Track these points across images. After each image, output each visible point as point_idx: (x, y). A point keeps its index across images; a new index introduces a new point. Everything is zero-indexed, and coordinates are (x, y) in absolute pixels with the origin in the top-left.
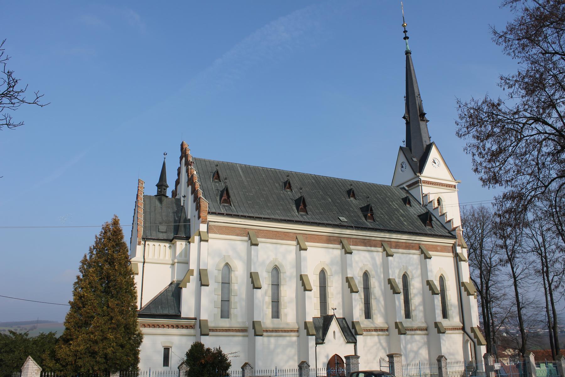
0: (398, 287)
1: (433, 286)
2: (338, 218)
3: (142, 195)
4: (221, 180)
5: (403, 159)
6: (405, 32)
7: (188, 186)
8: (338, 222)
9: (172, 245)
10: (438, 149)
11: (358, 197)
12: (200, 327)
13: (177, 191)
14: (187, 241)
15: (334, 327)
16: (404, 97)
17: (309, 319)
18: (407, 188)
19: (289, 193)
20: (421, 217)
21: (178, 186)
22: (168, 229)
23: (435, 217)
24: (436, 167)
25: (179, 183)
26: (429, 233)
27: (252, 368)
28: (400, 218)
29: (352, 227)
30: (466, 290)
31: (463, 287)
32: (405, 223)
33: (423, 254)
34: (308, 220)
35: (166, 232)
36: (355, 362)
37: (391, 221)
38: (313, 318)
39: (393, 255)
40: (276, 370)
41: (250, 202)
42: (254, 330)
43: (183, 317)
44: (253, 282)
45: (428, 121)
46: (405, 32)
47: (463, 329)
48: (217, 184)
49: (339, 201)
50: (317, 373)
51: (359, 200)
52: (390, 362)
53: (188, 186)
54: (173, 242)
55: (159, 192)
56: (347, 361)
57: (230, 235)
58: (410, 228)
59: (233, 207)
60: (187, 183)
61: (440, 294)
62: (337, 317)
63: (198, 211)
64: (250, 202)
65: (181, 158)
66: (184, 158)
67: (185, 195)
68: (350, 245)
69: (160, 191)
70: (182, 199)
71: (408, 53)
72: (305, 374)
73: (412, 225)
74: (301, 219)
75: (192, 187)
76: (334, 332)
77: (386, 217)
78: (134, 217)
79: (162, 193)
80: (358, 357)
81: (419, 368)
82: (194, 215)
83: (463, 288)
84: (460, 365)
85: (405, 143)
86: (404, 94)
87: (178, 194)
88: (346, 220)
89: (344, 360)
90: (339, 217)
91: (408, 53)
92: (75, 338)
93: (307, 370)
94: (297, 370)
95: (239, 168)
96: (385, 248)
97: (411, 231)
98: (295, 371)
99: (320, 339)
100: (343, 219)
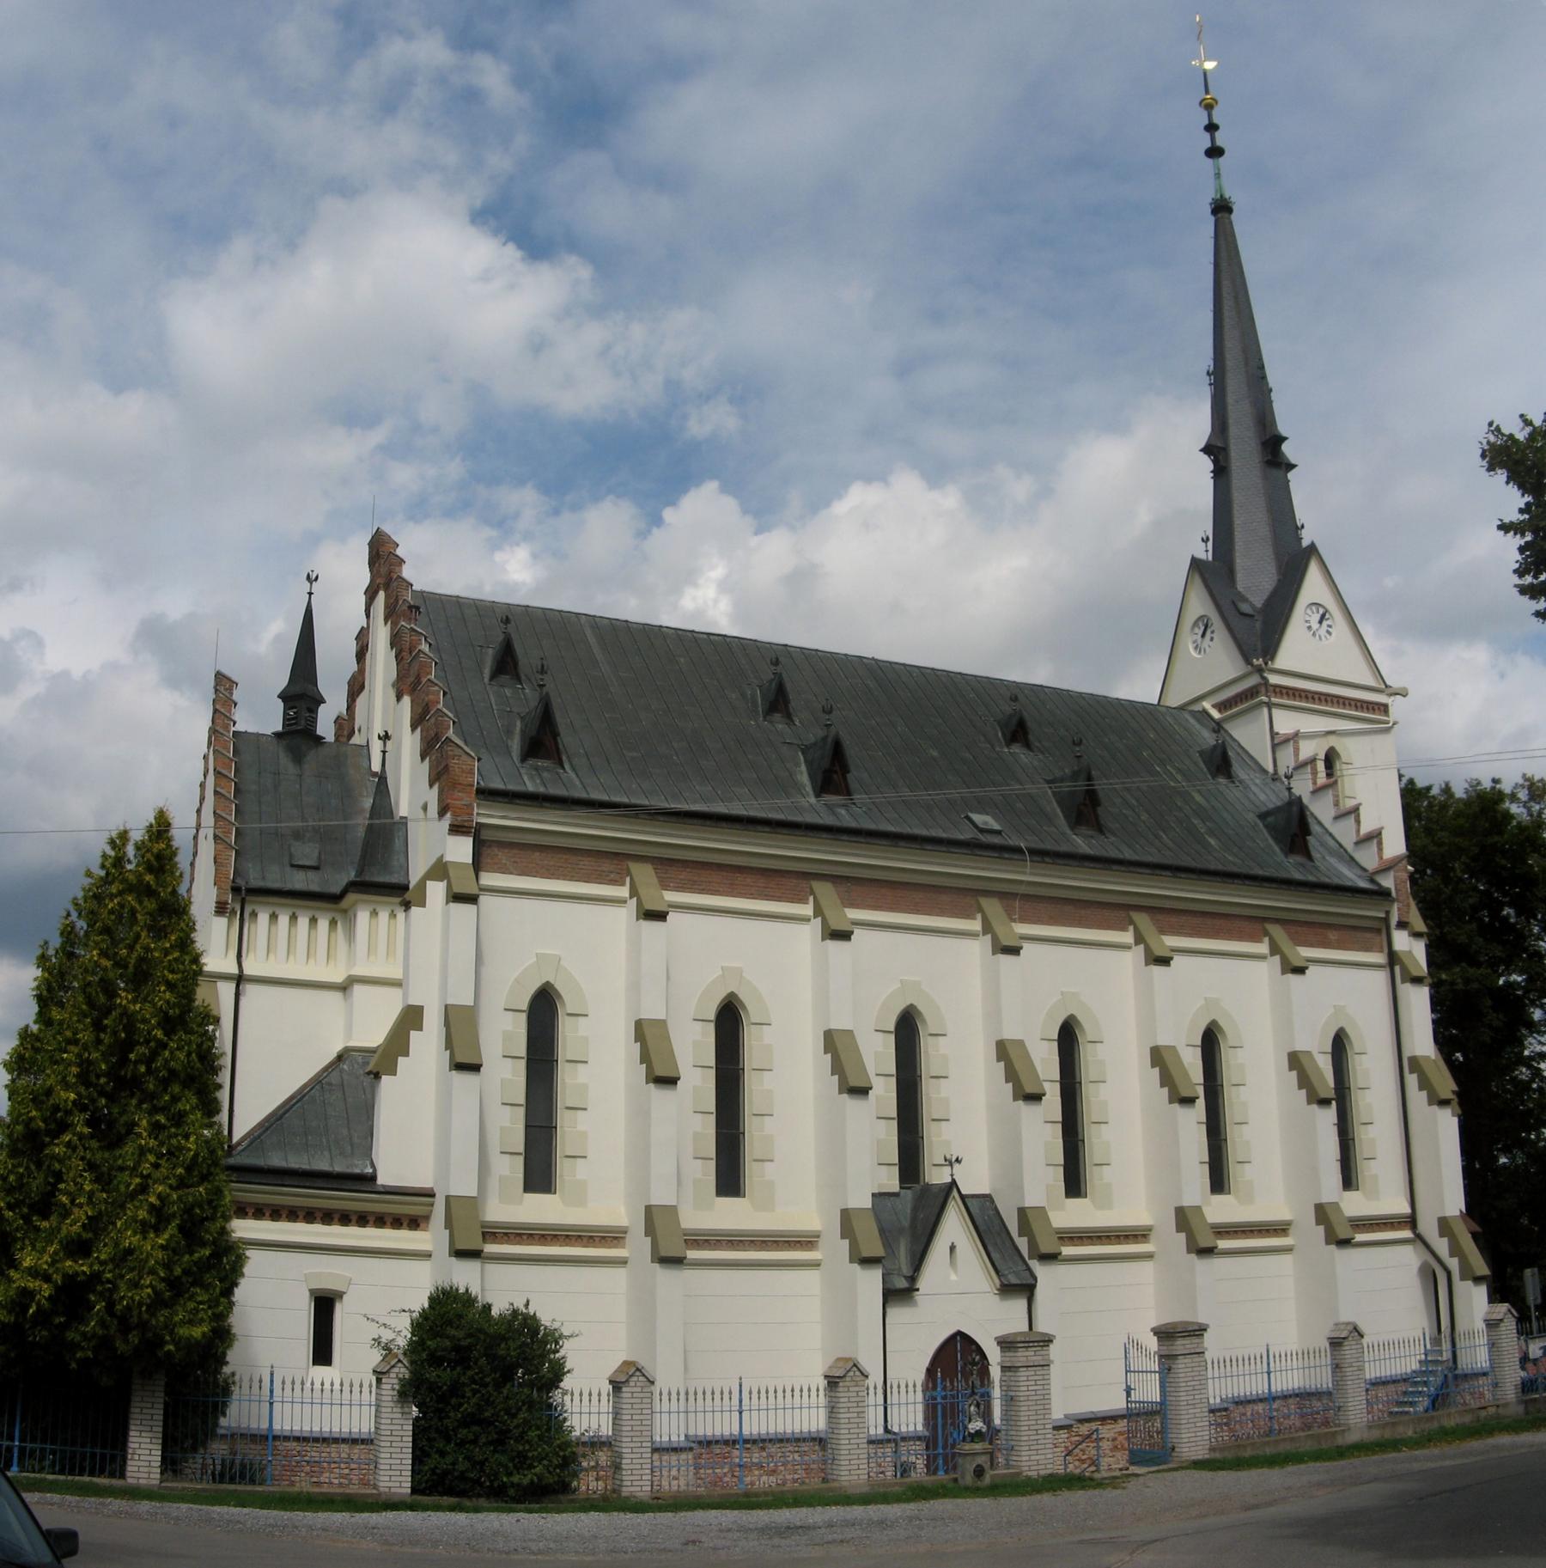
0: (1186, 1074)
1: (1309, 1072)
2: (968, 818)
3: (229, 732)
4: (523, 677)
5: (1200, 604)
6: (1212, 128)
7: (399, 698)
8: (966, 834)
9: (338, 917)
10: (1326, 567)
11: (1040, 742)
12: (449, 1224)
13: (354, 719)
14: (400, 899)
15: (954, 1227)
16: (1208, 373)
17: (862, 1200)
18: (1216, 714)
19: (780, 726)
20: (1270, 819)
21: (361, 701)
22: (323, 857)
23: (1320, 823)
24: (1320, 636)
25: (362, 687)
26: (1297, 876)
27: (649, 1381)
28: (1196, 822)
29: (1018, 850)
30: (1424, 1084)
31: (1415, 1076)
32: (1212, 841)
33: (1142, 946)
34: (853, 824)
35: (316, 868)
36: (1035, 1358)
37: (1162, 834)
38: (873, 1195)
39: (1021, 948)
40: (741, 1391)
41: (635, 754)
42: (649, 1239)
43: (383, 1186)
44: (645, 1057)
45: (1291, 467)
46: (1212, 128)
47: (1411, 1221)
48: (508, 692)
49: (968, 755)
50: (889, 1402)
51: (1042, 753)
52: (1163, 1353)
53: (399, 698)
54: (345, 903)
55: (289, 720)
56: (1007, 1354)
57: (558, 879)
58: (1230, 858)
59: (572, 775)
60: (393, 686)
61: (1334, 1102)
62: (963, 1192)
63: (439, 788)
64: (635, 754)
65: (371, 594)
66: (382, 594)
67: (386, 732)
68: (1014, 921)
69: (293, 719)
70: (376, 747)
71: (1222, 208)
72: (849, 1405)
73: (1235, 850)
74: (828, 820)
75: (412, 701)
76: (952, 1248)
77: (1144, 817)
78: (199, 811)
79: (303, 722)
80: (1047, 1341)
81: (1265, 1370)
82: (421, 804)
83: (1412, 1080)
84: (1397, 1355)
85: (1210, 544)
86: (1206, 360)
87: (359, 731)
88: (997, 827)
89: (994, 1354)
90: (970, 815)
91: (1222, 208)
92: (119, 1113)
93: (857, 1389)
94: (818, 1390)
95: (589, 633)
96: (990, 924)
97: (1236, 870)
98: (813, 1393)
99: (899, 1275)
100: (986, 823)
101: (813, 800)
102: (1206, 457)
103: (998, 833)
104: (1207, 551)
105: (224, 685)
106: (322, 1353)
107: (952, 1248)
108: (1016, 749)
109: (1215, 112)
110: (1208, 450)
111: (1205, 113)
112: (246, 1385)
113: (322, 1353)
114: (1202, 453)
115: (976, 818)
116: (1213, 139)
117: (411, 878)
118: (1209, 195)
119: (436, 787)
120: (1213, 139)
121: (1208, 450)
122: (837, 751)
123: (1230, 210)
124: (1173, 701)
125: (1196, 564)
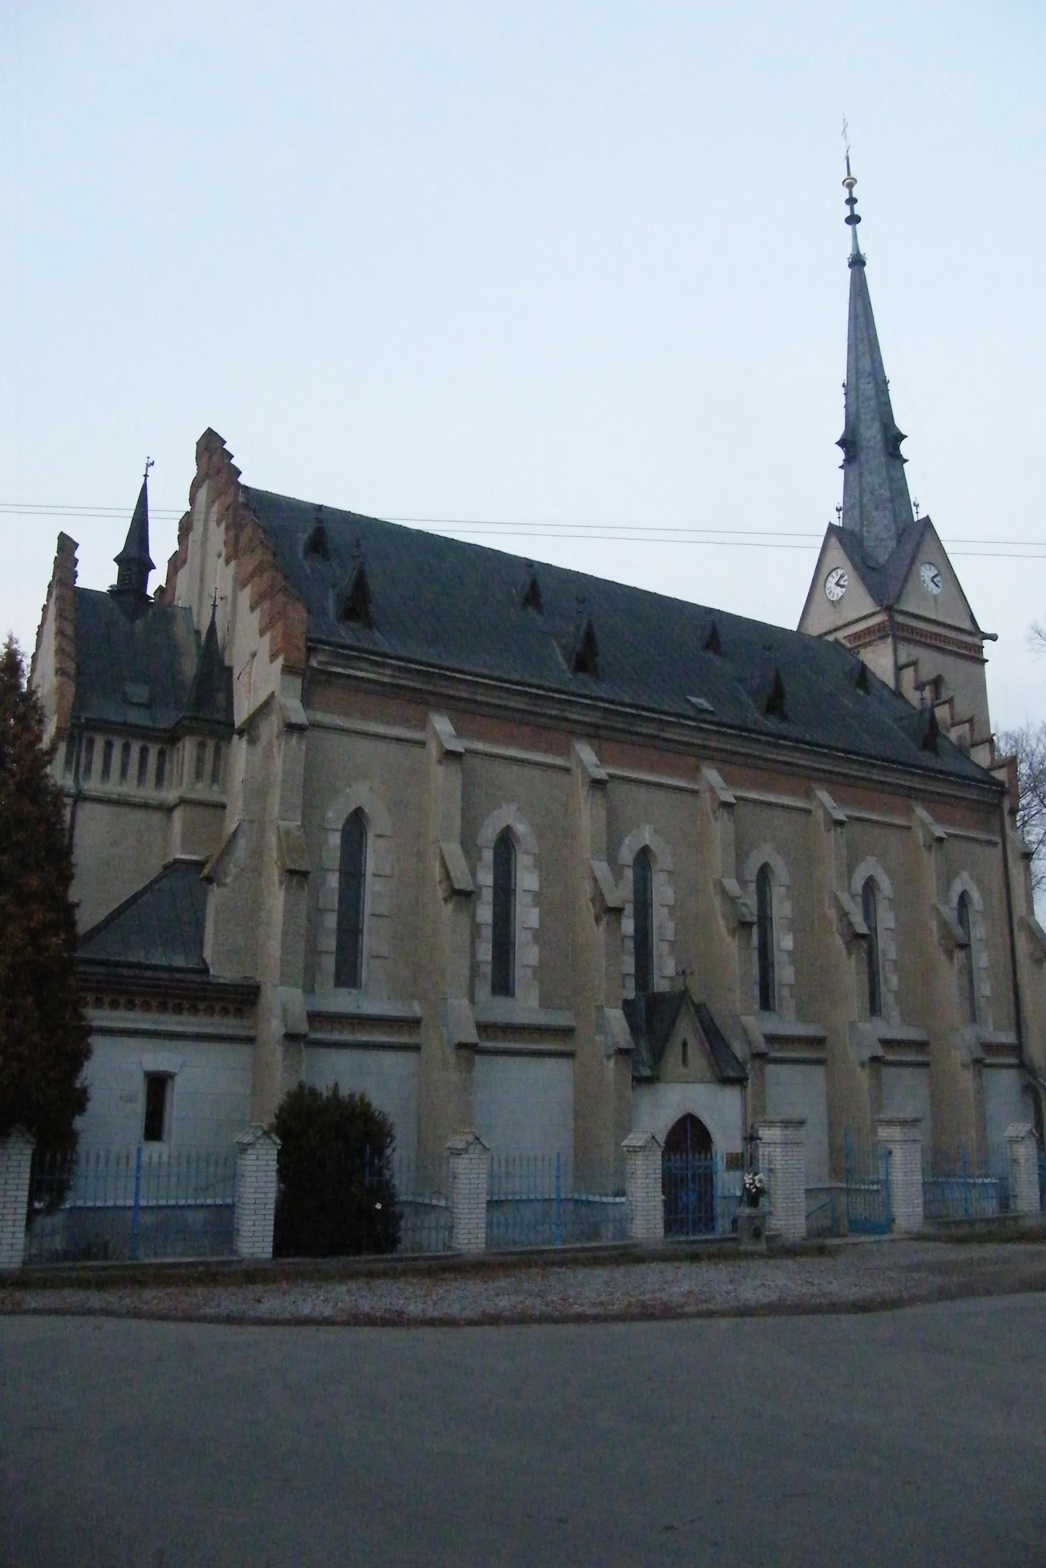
6: (851, 201)
46: (851, 201)
71: (857, 262)
88: (712, 709)
91: (857, 262)
101: (570, 676)
102: (840, 448)
103: (712, 712)
104: (839, 518)
105: (66, 546)
106: (154, 1130)
107: (685, 1044)
108: (710, 655)
109: (854, 190)
110: (842, 443)
111: (847, 191)
112: (92, 1159)
113: (154, 1130)
114: (837, 446)
115: (694, 700)
116: (852, 210)
117: (236, 718)
118: (848, 252)
119: (268, 637)
120: (852, 210)
121: (842, 443)
122: (590, 639)
123: (864, 264)
124: (814, 629)
125: (831, 528)
